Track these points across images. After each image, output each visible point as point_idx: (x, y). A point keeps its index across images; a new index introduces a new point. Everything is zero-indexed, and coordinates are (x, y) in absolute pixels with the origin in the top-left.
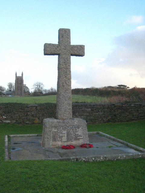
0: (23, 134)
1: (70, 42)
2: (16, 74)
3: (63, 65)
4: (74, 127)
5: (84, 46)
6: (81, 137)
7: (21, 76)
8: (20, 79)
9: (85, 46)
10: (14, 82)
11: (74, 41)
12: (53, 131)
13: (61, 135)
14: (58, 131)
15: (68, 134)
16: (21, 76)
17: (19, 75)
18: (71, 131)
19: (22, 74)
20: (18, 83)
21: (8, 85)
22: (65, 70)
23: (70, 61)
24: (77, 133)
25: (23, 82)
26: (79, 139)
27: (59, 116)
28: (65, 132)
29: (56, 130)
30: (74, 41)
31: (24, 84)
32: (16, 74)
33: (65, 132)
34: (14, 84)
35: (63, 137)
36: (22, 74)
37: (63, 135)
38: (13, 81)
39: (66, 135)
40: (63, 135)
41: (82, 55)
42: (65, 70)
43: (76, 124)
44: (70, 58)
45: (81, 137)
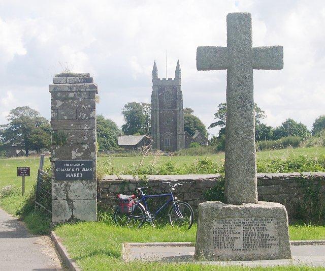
0: (88, 162)
1: (251, 42)
2: (155, 72)
3: (236, 91)
4: (259, 219)
5: (282, 47)
6: (274, 242)
7: (173, 77)
8: (170, 91)
9: (284, 50)
10: (148, 101)
11: (260, 38)
12: (215, 227)
13: (232, 235)
14: (226, 227)
15: (246, 237)
16: (173, 77)
17: (167, 73)
18: (253, 229)
19: (178, 71)
20: (161, 103)
21: (124, 113)
22: (239, 100)
23: (252, 81)
24: (266, 233)
25: (181, 101)
26: (269, 246)
27: (230, 198)
28: (240, 229)
29: (221, 226)
30: (260, 38)
31: (185, 106)
32: (155, 72)
33: (240, 229)
34: (146, 112)
35: (237, 241)
36: (178, 71)
37: (235, 236)
38: (144, 97)
39: (241, 236)
40: (235, 236)
41: (279, 66)
42: (239, 100)
43: (77, 158)
44: (252, 73)
45: (274, 242)
